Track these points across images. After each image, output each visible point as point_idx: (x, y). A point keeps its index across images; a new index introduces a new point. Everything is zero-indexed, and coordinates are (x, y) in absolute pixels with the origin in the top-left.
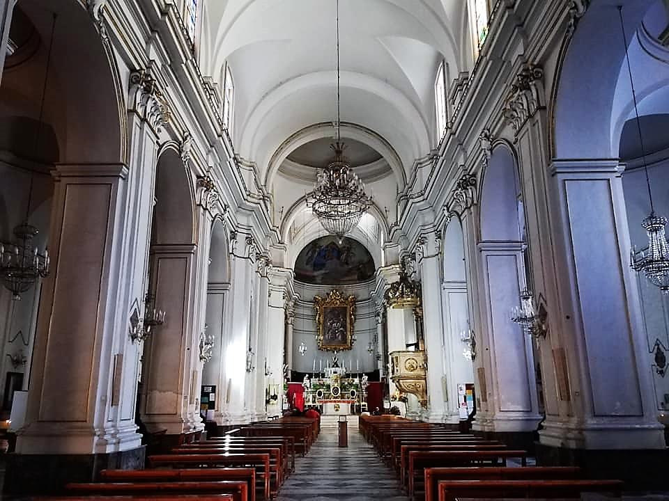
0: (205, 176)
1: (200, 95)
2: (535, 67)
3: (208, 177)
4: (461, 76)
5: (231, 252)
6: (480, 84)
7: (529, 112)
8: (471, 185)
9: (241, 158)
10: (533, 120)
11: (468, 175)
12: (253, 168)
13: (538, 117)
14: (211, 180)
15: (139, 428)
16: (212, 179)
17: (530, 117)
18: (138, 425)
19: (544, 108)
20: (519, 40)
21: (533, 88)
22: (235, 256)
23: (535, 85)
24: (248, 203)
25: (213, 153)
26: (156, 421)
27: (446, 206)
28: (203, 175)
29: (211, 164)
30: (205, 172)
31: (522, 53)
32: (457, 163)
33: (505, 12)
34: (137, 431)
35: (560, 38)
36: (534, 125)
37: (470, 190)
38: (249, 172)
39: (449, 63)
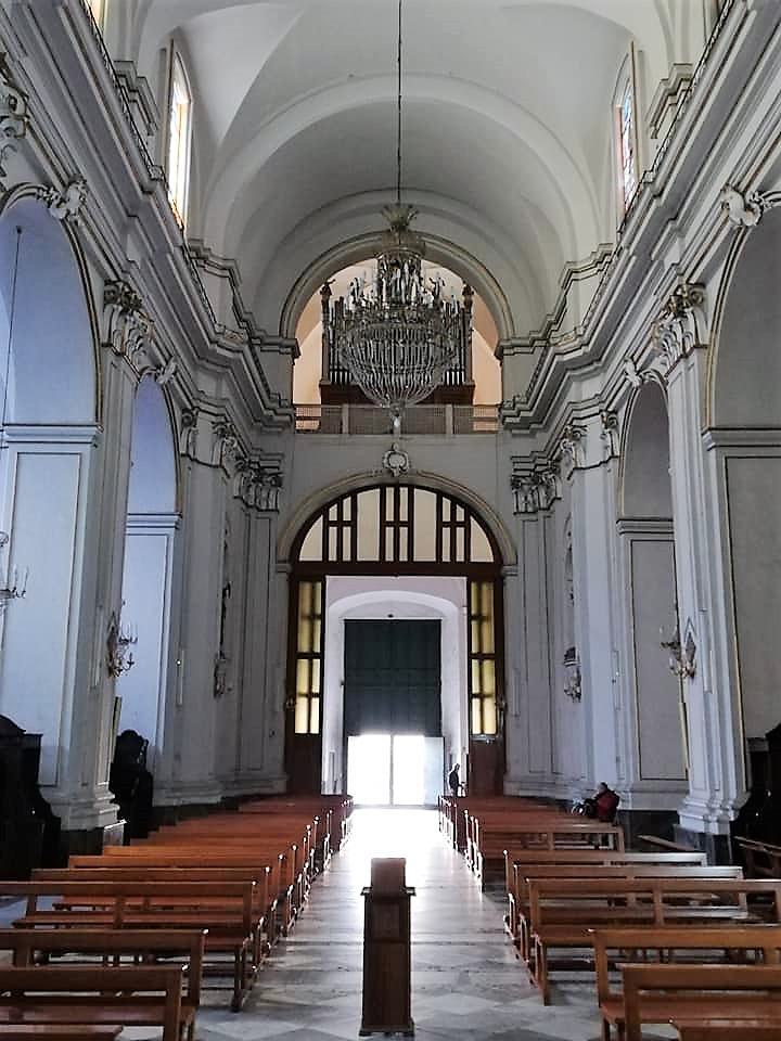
0: (119, 280)
1: (98, 84)
2: (611, 413)
3: (126, 284)
4: (601, 250)
5: (183, 451)
6: (596, 334)
7: (684, 349)
8: (237, 997)
9: (205, 250)
10: (688, 363)
11: (606, 410)
12: (231, 276)
13: (694, 358)
14: (131, 291)
15: (114, 796)
16: (134, 288)
17: (685, 356)
18: (113, 793)
19: (705, 347)
20: (674, 240)
21: (690, 316)
22: (192, 460)
23: (693, 313)
24: (219, 350)
25: (137, 232)
26: (426, 890)
27: (736, 189)
28: (114, 278)
29: (133, 254)
30: (119, 273)
31: (677, 262)
32: (661, 263)
33: (650, 203)
34: (112, 801)
35: (718, 266)
36: (689, 369)
37: (690, 316)
38: (219, 279)
39: (645, 49)
